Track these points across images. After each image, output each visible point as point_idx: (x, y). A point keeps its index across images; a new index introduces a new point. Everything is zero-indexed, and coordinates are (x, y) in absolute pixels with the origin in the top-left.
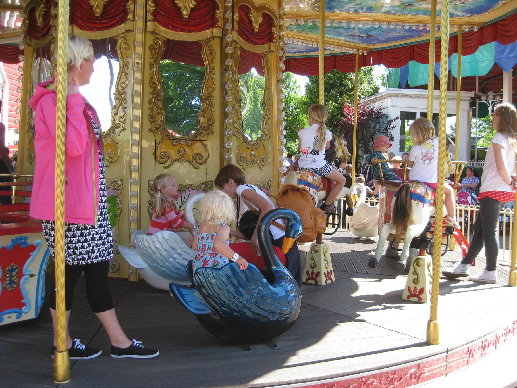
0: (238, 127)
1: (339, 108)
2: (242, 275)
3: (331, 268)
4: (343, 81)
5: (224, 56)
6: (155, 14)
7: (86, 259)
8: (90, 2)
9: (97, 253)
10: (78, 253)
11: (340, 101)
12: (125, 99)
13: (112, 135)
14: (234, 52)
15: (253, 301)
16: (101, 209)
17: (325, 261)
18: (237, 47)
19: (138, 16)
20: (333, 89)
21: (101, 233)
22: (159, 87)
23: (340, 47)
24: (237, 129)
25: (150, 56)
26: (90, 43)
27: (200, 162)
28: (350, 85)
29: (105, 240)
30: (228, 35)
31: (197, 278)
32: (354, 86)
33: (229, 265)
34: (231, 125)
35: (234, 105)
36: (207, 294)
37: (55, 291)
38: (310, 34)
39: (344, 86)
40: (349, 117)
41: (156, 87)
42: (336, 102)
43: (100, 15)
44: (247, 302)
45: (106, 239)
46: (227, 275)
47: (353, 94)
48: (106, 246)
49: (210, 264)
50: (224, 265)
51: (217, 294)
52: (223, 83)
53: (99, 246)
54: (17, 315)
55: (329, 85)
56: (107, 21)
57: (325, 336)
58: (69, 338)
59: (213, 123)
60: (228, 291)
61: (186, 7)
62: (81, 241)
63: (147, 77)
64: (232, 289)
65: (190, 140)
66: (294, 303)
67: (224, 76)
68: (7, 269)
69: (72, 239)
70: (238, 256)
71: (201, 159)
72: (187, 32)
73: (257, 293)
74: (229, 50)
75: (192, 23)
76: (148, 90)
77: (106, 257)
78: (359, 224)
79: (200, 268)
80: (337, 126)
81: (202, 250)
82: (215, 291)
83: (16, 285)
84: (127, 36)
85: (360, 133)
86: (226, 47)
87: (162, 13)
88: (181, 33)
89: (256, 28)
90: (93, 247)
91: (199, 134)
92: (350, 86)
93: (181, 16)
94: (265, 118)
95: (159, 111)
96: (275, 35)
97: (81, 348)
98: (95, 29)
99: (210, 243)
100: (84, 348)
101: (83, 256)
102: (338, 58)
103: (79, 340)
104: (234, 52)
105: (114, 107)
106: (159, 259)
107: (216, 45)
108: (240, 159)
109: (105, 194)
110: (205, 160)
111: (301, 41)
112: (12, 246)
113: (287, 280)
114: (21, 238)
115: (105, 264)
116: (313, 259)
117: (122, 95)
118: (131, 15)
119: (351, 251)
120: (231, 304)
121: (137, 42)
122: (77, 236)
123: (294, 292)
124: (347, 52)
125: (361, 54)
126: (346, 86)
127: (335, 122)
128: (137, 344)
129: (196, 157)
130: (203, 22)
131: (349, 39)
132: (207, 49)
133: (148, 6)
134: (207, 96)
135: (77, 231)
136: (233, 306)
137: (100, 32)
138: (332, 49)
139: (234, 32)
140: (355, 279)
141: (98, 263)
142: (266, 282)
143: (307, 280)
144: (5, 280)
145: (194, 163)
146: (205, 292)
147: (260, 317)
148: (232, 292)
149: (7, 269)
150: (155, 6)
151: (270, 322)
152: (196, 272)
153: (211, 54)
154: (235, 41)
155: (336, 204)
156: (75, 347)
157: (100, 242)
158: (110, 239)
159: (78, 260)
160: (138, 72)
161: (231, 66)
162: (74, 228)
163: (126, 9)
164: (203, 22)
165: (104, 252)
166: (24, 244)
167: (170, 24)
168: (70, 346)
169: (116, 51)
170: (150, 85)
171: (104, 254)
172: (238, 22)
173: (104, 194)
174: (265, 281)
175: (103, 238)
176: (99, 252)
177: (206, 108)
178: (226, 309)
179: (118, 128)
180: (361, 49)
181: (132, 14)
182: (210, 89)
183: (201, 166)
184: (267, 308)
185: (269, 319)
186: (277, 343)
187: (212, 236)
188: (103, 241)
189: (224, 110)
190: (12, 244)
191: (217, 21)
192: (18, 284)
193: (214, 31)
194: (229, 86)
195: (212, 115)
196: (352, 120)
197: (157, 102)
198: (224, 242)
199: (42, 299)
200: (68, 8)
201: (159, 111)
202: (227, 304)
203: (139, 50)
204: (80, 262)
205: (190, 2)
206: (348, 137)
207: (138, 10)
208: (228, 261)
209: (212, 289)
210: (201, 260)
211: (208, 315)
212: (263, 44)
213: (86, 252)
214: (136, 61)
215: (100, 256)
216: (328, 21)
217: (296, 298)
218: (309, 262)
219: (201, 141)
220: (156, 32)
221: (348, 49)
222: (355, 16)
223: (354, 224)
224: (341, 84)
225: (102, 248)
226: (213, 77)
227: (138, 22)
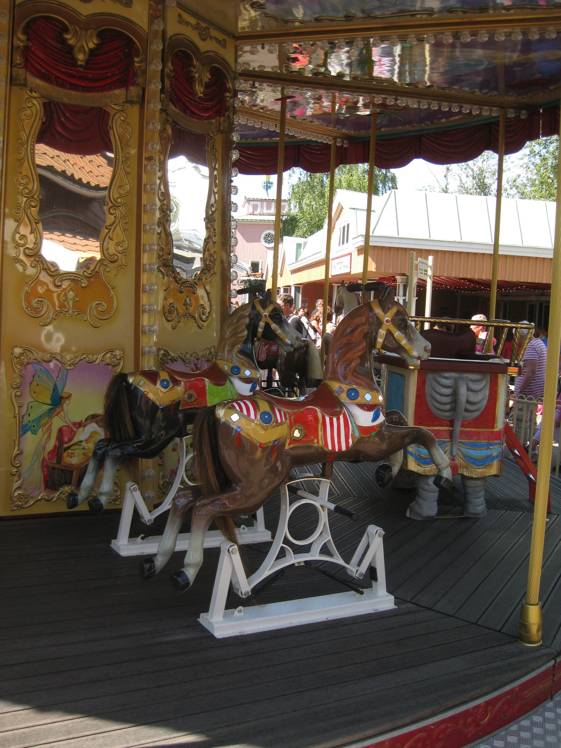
89: (199, 90)
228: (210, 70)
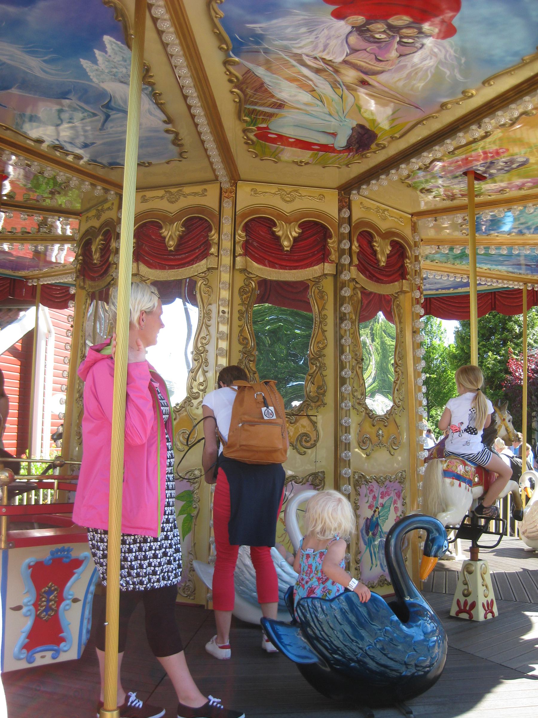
0: (359, 397)
1: (503, 362)
2: (363, 611)
3: (491, 596)
4: (507, 324)
5: (339, 301)
6: (246, 246)
7: (145, 583)
8: (161, 232)
9: (159, 575)
10: (135, 574)
11: (503, 352)
12: (206, 360)
13: (188, 408)
14: (353, 294)
15: (378, 646)
16: (168, 515)
17: (483, 585)
18: (357, 288)
19: (224, 250)
20: (494, 335)
21: (166, 548)
22: (252, 344)
23: (500, 281)
24: (359, 399)
25: (240, 302)
26: (154, 289)
27: (308, 445)
28: (517, 329)
29: (172, 558)
30: (344, 272)
31: (299, 611)
32: (522, 332)
33: (344, 595)
34: (349, 394)
35: (353, 366)
36: (313, 635)
37: (104, 627)
38: (458, 264)
39: (508, 331)
40: (517, 374)
41: (247, 343)
42: (498, 354)
43: (174, 249)
44: (369, 648)
45: (173, 556)
46: (341, 609)
47: (522, 342)
48: (172, 566)
49: (318, 593)
50: (337, 594)
51: (328, 636)
52: (339, 337)
53: (163, 566)
54: (53, 654)
55: (487, 330)
56: (183, 256)
57: (483, 700)
58: (121, 691)
59: (325, 391)
60: (343, 632)
61: (287, 237)
62: (139, 558)
63: (236, 330)
64: (348, 629)
65: (294, 415)
66: (436, 650)
67: (340, 328)
68: (43, 590)
69: (127, 555)
70: (357, 582)
71: (308, 442)
72: (289, 269)
73: (383, 636)
74: (346, 292)
75: (296, 257)
76: (237, 347)
77: (172, 581)
78: (534, 529)
79: (304, 598)
80: (500, 387)
81: (306, 573)
82: (324, 631)
83: (53, 613)
84: (210, 276)
85: (533, 397)
86: (341, 289)
87: (255, 244)
88: (281, 271)
89: (383, 260)
90: (155, 566)
91: (305, 407)
92: (517, 331)
93: (281, 248)
94: (396, 384)
95: (252, 376)
96: (409, 270)
97: (137, 705)
98: (167, 267)
99: (318, 564)
100: (141, 706)
101: (141, 578)
102: (498, 295)
103: (135, 694)
104: (353, 294)
105: (192, 371)
106: (248, 580)
107: (328, 285)
108: (363, 442)
109: (173, 495)
110: (313, 443)
111: (446, 274)
112: (50, 560)
113: (427, 617)
114: (63, 550)
115: (172, 590)
116: (466, 584)
117: (202, 355)
118: (214, 249)
119: (522, 570)
120: (347, 651)
121: (223, 283)
122: (134, 551)
123: (437, 635)
124: (511, 287)
125: (530, 289)
126: (511, 331)
127: (497, 382)
128: (214, 702)
129: (302, 439)
130: (311, 255)
131: (513, 269)
132: (317, 291)
133: (237, 236)
134: (316, 354)
135: (133, 544)
136: (349, 654)
137: (174, 270)
138: (489, 284)
139: (352, 268)
140: (527, 613)
141: (161, 589)
142: (397, 620)
143: (458, 613)
144: (40, 605)
145: (299, 446)
146: (310, 632)
147: (388, 671)
148: (348, 633)
149: (43, 590)
150: (246, 236)
151: (401, 678)
152: (299, 604)
153: (322, 298)
154: (354, 280)
155: (499, 504)
156: (129, 704)
157: (164, 560)
158: (178, 556)
159: (134, 583)
160: (223, 323)
161: (349, 313)
162: (130, 539)
163: (208, 240)
164: (311, 255)
165: (170, 574)
166: (67, 557)
167: (266, 259)
168: (122, 702)
169: (195, 295)
170: (239, 340)
171: (169, 577)
172: (358, 254)
173: (171, 494)
174: (395, 618)
175: (169, 555)
176: (163, 574)
177: (314, 372)
178: (340, 658)
179: (195, 398)
180: (530, 283)
181: (216, 247)
182: (321, 346)
183: (309, 451)
184: (398, 658)
185: (401, 673)
186: (413, 709)
187: (322, 554)
188: (168, 558)
189: (340, 373)
190: (51, 557)
191: (329, 253)
192: (57, 612)
193: (325, 267)
194: (347, 341)
195: (323, 380)
196: (521, 380)
197: (249, 364)
198: (335, 564)
199: (88, 632)
200: (132, 240)
201: (252, 376)
202: (342, 651)
203: (225, 294)
204: (137, 587)
205: (292, 230)
206: (517, 402)
207: (223, 242)
208: (343, 589)
209: (320, 629)
210: (306, 586)
211: (314, 664)
212: (392, 282)
213: (145, 573)
214: (222, 309)
215: (164, 579)
216: (482, 247)
217: (439, 644)
218: (460, 588)
219: (308, 416)
220: (248, 270)
221: (511, 282)
222: (520, 239)
223: (526, 530)
224: (504, 329)
225: (166, 568)
226: (325, 329)
227: (223, 257)
228: (390, 243)
